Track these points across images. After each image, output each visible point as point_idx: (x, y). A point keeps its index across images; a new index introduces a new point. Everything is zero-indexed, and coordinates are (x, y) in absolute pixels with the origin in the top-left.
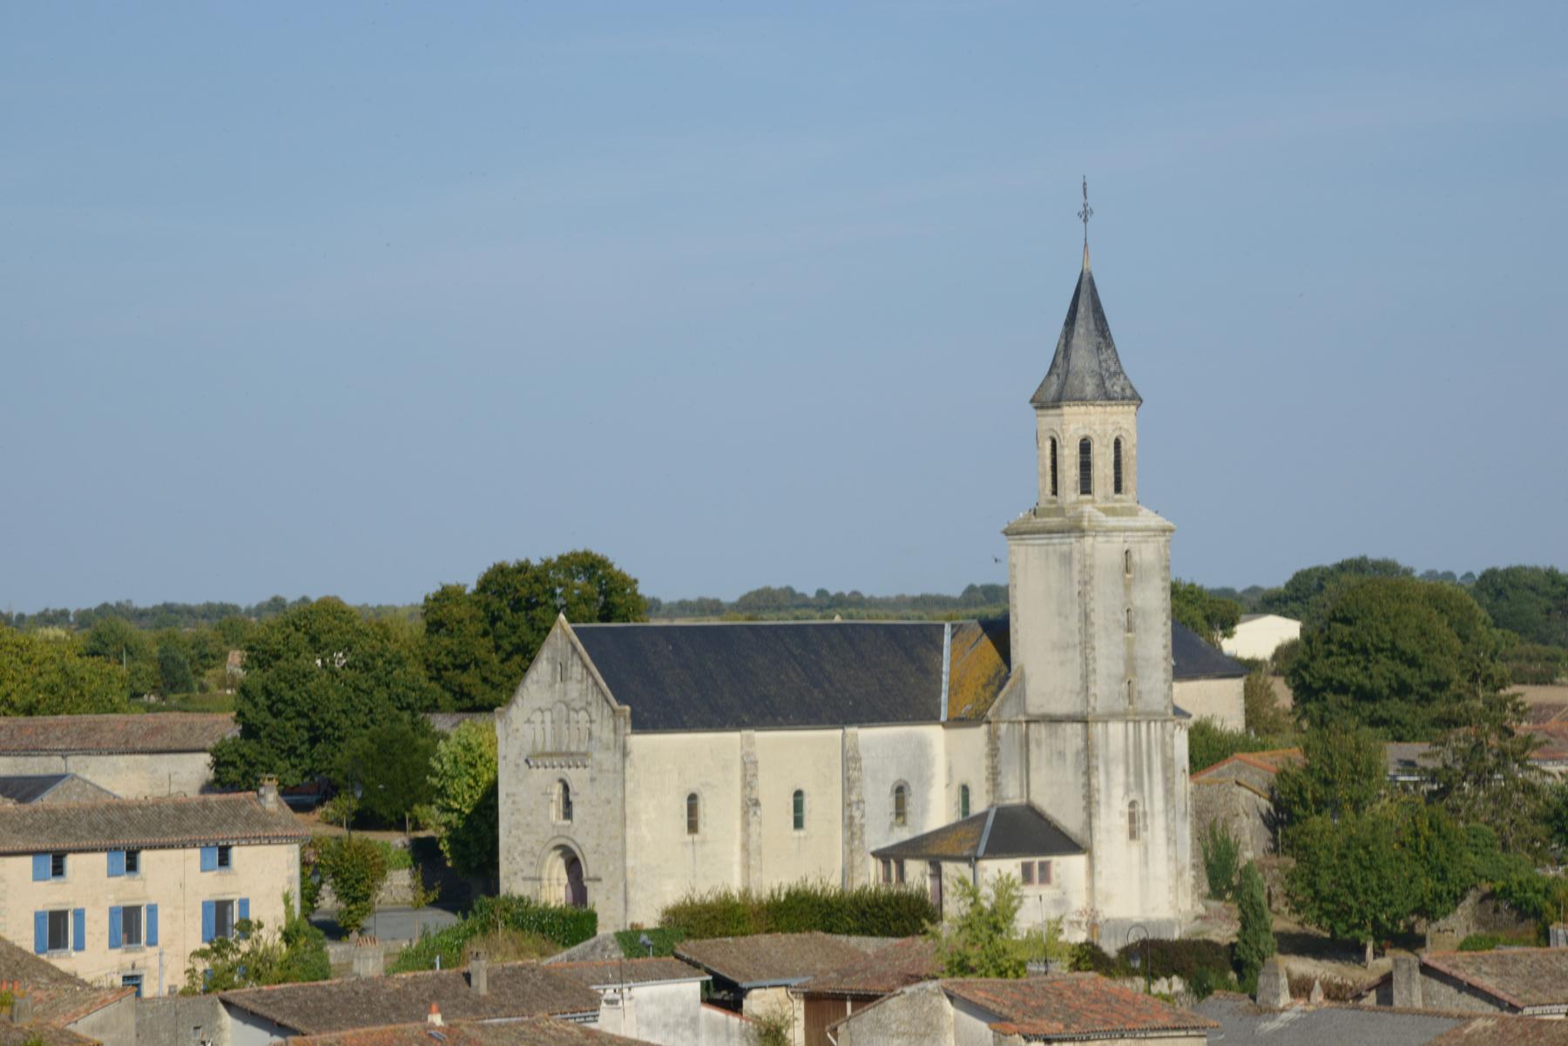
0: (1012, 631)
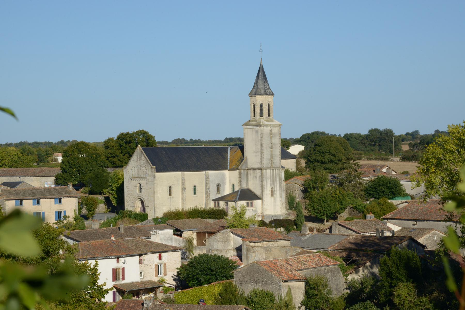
0: (244, 148)
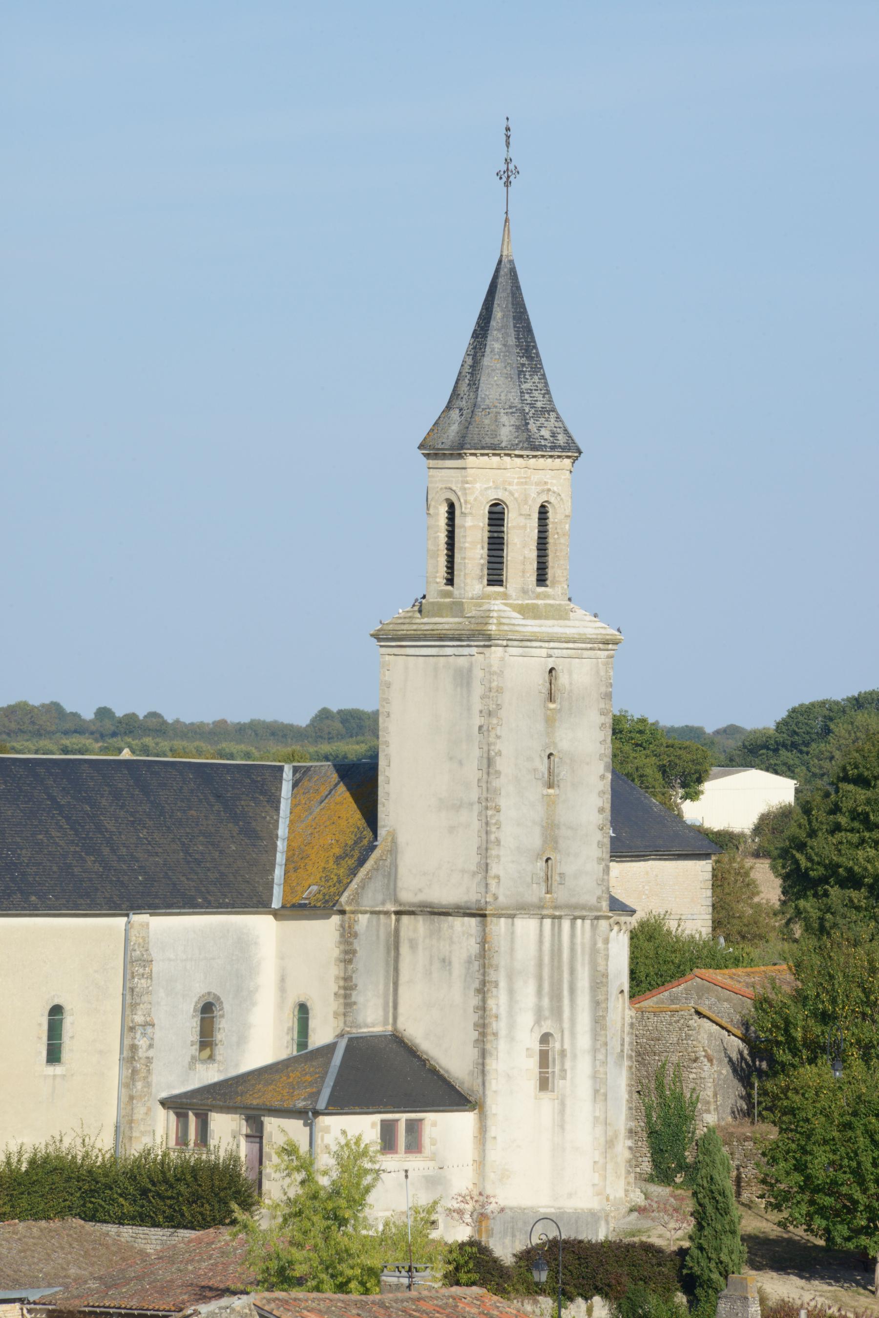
0: (381, 779)
